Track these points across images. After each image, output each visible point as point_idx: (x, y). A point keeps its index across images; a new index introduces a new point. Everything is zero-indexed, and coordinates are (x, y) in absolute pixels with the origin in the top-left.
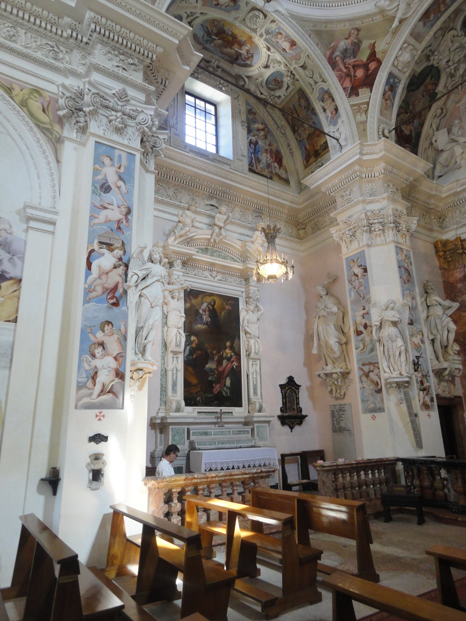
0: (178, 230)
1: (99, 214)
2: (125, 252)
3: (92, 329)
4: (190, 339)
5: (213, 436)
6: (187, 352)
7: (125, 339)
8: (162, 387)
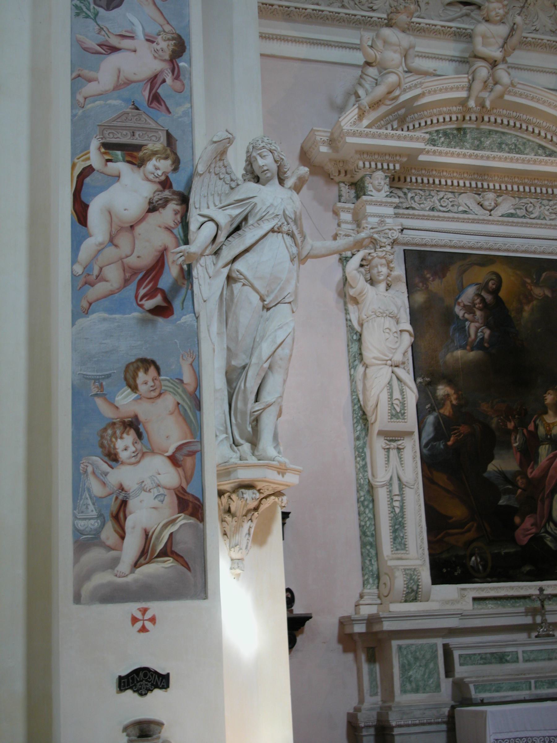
0: (367, 86)
1: (97, 70)
2: (176, 163)
3: (101, 385)
4: (434, 392)
5: (522, 665)
6: (429, 430)
7: (198, 404)
8: (363, 533)
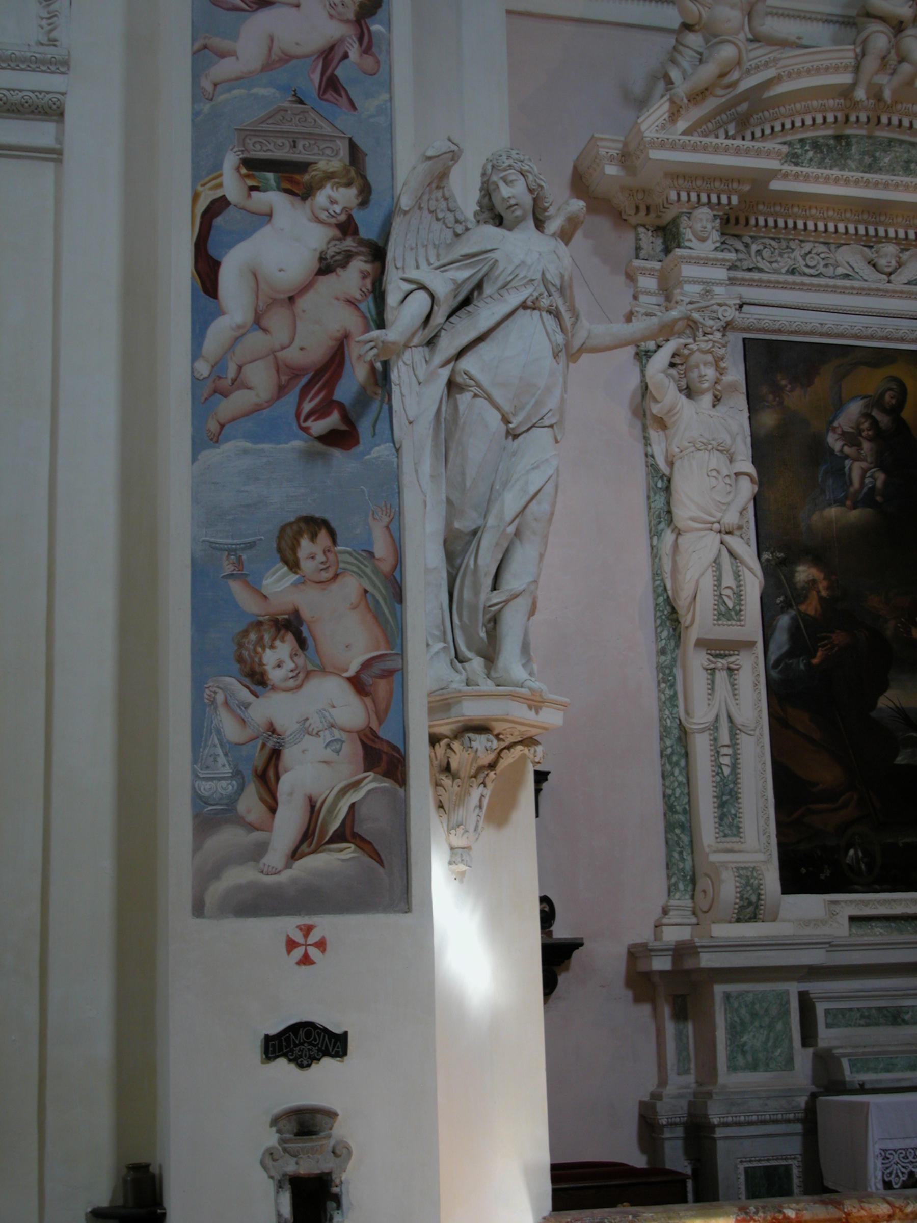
0: (685, 64)
2: (365, 194)
3: (239, 559)
6: (781, 638)
7: (397, 593)
8: (670, 808)
